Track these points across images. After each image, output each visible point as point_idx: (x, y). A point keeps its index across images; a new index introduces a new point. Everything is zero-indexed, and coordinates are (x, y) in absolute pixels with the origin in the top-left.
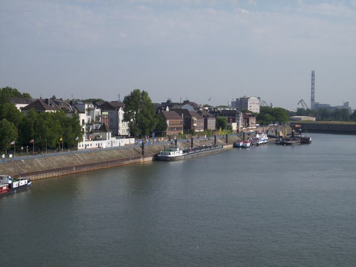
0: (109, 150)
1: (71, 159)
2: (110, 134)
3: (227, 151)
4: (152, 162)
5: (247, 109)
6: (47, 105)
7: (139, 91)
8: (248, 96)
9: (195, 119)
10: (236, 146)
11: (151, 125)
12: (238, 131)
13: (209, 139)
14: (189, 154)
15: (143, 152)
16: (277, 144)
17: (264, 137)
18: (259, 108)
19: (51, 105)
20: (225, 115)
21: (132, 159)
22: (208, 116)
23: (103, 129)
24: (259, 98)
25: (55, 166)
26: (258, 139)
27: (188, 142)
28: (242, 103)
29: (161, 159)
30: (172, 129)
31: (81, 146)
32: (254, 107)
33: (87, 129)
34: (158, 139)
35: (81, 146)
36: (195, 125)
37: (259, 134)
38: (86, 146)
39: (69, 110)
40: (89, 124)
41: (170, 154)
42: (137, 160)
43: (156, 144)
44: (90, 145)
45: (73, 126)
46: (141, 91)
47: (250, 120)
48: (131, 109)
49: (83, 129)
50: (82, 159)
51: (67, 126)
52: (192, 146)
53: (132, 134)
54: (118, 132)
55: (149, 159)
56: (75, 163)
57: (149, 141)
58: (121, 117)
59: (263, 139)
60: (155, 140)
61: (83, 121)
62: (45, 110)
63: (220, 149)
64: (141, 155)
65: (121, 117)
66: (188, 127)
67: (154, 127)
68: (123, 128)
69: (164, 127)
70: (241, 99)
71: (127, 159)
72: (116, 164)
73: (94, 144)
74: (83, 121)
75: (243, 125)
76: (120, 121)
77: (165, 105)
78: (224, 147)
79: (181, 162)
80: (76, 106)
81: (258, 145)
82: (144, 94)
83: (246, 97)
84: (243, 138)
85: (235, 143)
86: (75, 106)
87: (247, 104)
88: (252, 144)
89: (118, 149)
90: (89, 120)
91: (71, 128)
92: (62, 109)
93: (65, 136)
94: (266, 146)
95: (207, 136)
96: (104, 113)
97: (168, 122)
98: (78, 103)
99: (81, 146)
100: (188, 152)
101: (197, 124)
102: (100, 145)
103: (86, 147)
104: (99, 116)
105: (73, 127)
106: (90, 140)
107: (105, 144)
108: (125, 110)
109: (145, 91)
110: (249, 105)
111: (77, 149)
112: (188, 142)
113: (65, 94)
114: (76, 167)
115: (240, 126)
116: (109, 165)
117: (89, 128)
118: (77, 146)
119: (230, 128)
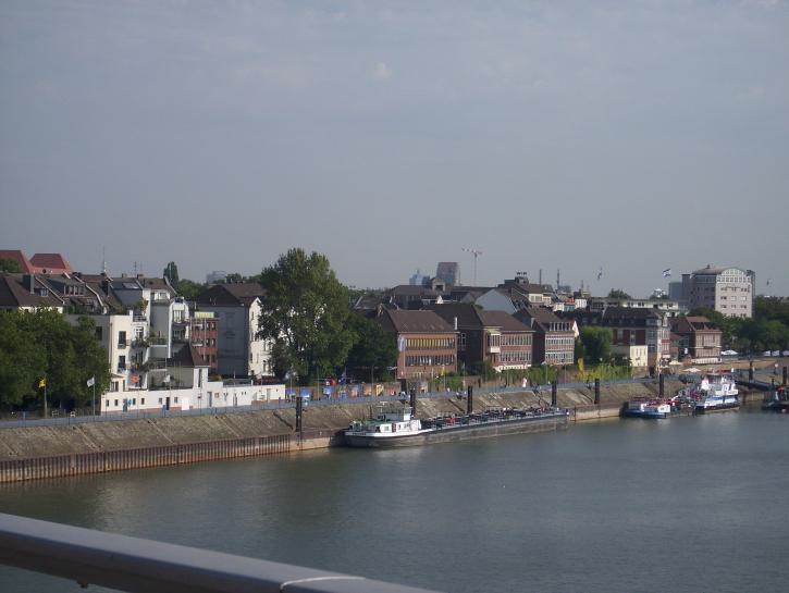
0: (191, 416)
1: (67, 437)
2: (205, 372)
3: (596, 427)
4: (327, 450)
5: (713, 306)
6: (24, 291)
7: (300, 252)
8: (717, 268)
9: (494, 332)
10: (628, 413)
11: (334, 349)
12: (652, 369)
13: (535, 392)
14: (442, 431)
15: (298, 423)
16: (765, 409)
17: (727, 389)
18: (749, 304)
19: (37, 291)
20: (615, 324)
21: (262, 441)
22: (547, 326)
23: (185, 357)
24: (750, 273)
25: (17, 452)
26: (704, 393)
27: (459, 397)
28: (697, 289)
29: (352, 443)
30: (413, 361)
31: (111, 402)
32: (734, 301)
33: (133, 359)
34: (362, 390)
35: (112, 403)
36: (494, 350)
37: (711, 379)
38: (126, 403)
39: (92, 306)
40: (139, 345)
41: (378, 430)
42: (278, 446)
43: (348, 401)
44: (138, 401)
45: (79, 349)
46: (308, 255)
47: (698, 339)
48: (280, 302)
49: (518, 348)
50: (101, 438)
51: (61, 348)
52: (470, 409)
53: (277, 377)
54: (246, 367)
55: (319, 444)
56: (78, 448)
57: (335, 393)
58: (255, 326)
59: (719, 393)
60: (355, 392)
61: (123, 335)
62: (18, 305)
63: (555, 421)
64: (293, 432)
65: (255, 326)
66: (472, 358)
67: (344, 355)
68: (260, 354)
69: (390, 356)
70: (696, 274)
71: (244, 442)
72: (209, 455)
73: (152, 400)
74: (123, 335)
75: (672, 354)
76: (252, 337)
77: (412, 299)
78: (580, 415)
79: (416, 452)
80: (120, 294)
81: (701, 410)
82: (318, 261)
83: (712, 270)
84: (658, 389)
85: (626, 404)
86: (115, 296)
87: (714, 289)
88: (677, 408)
89: (222, 413)
90: (141, 334)
91: (71, 355)
92: (72, 302)
93: (54, 373)
94: (730, 416)
95: (530, 384)
96: (198, 315)
97: (402, 341)
98: (127, 285)
99: (112, 403)
100: (439, 425)
101: (506, 352)
102: (172, 404)
103: (125, 408)
104: (183, 322)
105: (78, 352)
106: (145, 386)
107: (185, 400)
108: (265, 305)
109: (320, 253)
110: (719, 293)
111: (98, 413)
112: (459, 397)
113: (83, 260)
114: (82, 458)
115: (659, 356)
116: (185, 457)
117: (141, 355)
118: (98, 402)
119: (623, 361)
